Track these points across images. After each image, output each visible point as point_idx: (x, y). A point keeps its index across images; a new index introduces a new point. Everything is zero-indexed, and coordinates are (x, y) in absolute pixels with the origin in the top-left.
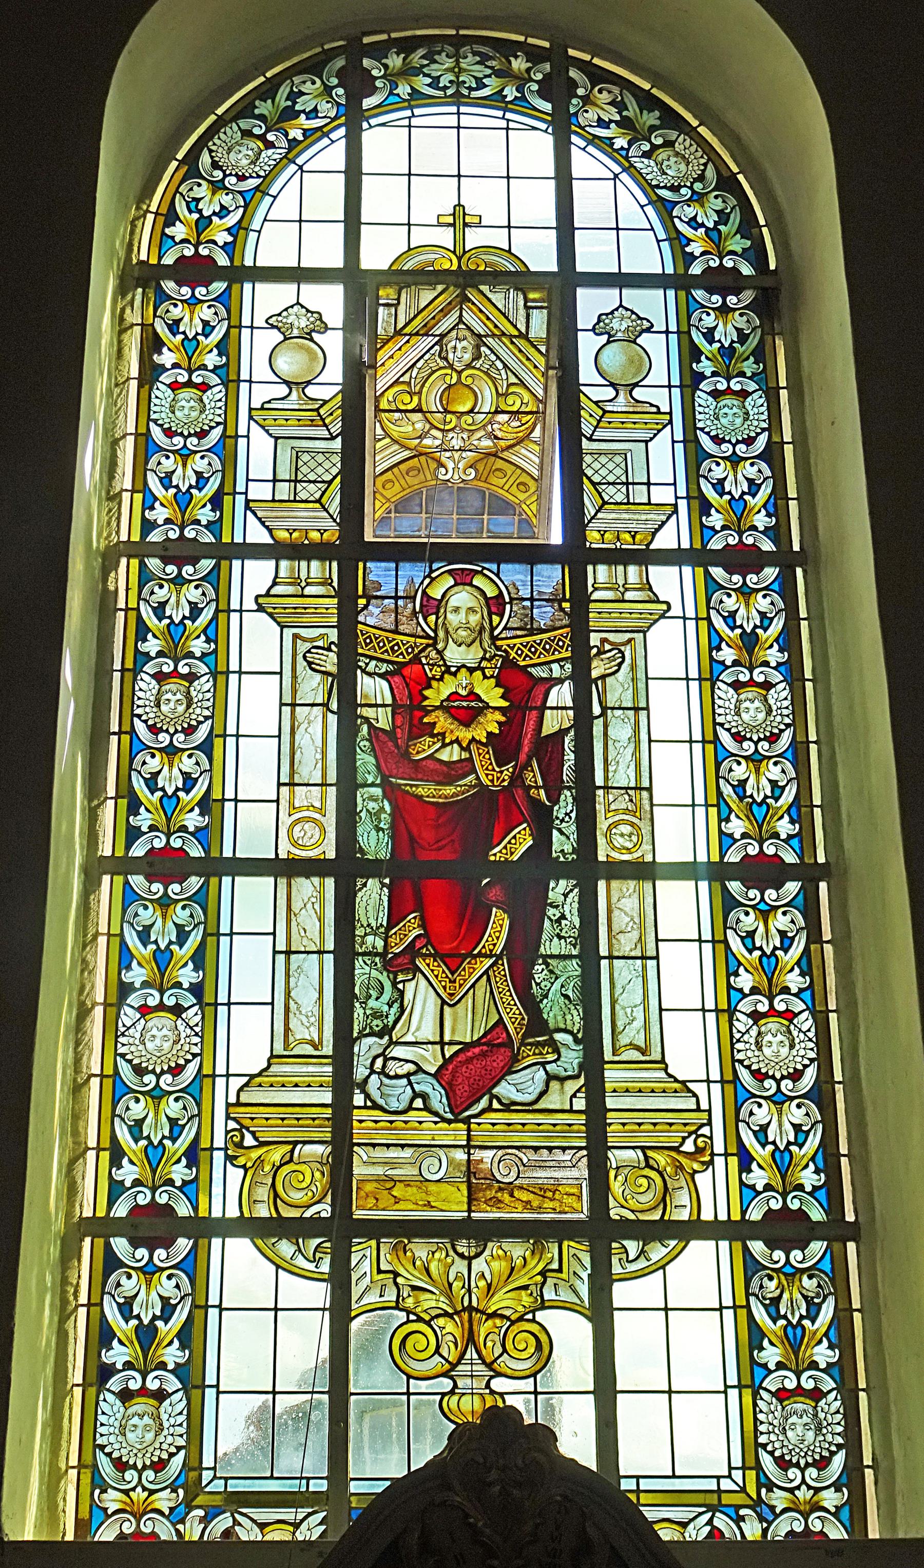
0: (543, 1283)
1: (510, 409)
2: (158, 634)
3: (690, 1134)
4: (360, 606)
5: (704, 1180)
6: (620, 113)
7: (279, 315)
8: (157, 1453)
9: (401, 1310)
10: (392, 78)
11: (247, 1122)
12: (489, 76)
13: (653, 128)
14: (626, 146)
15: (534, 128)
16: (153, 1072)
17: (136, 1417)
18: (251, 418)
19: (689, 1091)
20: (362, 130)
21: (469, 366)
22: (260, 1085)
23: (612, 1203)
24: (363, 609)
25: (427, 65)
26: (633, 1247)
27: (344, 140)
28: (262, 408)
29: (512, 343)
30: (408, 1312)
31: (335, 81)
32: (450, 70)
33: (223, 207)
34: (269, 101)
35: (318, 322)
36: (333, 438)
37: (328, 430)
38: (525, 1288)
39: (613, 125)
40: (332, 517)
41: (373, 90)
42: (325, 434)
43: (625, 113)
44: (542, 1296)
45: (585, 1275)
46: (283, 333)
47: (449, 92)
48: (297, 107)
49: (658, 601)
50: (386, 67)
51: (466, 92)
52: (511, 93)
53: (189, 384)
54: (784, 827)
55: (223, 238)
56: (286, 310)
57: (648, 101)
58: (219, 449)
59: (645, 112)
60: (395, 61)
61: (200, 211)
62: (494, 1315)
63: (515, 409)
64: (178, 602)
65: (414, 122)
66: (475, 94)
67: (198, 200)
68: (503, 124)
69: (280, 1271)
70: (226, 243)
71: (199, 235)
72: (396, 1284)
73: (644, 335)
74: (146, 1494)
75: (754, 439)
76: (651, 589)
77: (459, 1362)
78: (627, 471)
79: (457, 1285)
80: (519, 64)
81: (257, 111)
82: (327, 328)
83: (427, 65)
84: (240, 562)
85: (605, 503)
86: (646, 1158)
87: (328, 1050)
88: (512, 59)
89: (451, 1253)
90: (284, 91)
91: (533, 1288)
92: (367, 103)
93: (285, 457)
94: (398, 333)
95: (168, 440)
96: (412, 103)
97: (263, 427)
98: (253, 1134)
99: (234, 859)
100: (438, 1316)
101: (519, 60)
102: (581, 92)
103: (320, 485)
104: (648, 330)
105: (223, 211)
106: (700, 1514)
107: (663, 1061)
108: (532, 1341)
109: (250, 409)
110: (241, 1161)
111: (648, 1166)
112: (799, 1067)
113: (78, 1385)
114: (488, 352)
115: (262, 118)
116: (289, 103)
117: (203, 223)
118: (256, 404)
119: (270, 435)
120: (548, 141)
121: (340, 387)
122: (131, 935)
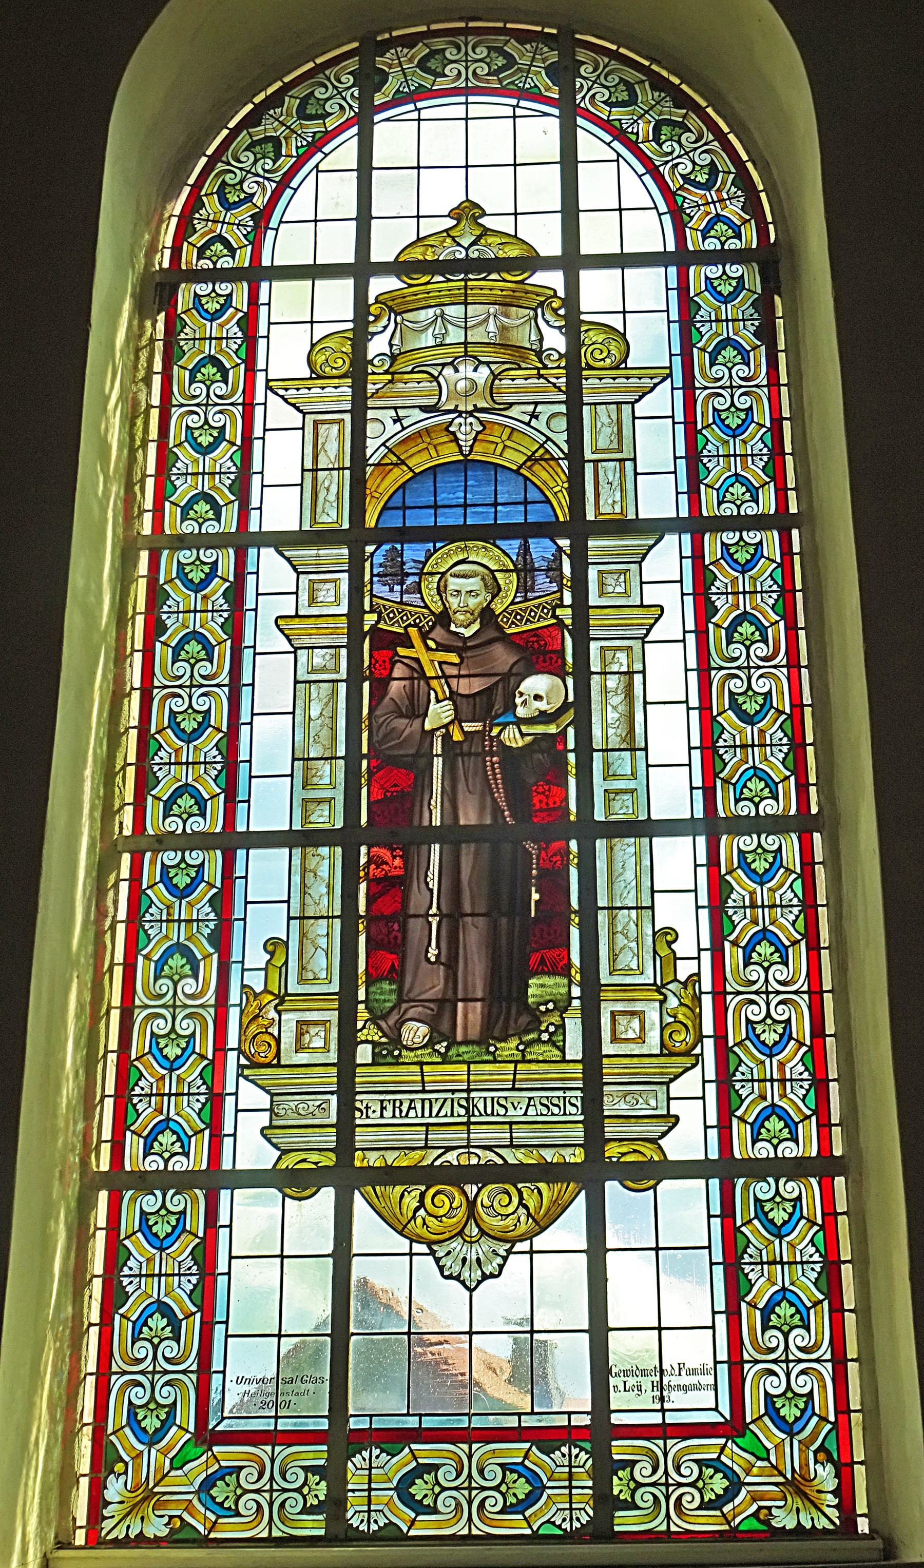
15: (546, 114)
69: (287, 1199)
99: (234, 1171)
113: (91, 1374)
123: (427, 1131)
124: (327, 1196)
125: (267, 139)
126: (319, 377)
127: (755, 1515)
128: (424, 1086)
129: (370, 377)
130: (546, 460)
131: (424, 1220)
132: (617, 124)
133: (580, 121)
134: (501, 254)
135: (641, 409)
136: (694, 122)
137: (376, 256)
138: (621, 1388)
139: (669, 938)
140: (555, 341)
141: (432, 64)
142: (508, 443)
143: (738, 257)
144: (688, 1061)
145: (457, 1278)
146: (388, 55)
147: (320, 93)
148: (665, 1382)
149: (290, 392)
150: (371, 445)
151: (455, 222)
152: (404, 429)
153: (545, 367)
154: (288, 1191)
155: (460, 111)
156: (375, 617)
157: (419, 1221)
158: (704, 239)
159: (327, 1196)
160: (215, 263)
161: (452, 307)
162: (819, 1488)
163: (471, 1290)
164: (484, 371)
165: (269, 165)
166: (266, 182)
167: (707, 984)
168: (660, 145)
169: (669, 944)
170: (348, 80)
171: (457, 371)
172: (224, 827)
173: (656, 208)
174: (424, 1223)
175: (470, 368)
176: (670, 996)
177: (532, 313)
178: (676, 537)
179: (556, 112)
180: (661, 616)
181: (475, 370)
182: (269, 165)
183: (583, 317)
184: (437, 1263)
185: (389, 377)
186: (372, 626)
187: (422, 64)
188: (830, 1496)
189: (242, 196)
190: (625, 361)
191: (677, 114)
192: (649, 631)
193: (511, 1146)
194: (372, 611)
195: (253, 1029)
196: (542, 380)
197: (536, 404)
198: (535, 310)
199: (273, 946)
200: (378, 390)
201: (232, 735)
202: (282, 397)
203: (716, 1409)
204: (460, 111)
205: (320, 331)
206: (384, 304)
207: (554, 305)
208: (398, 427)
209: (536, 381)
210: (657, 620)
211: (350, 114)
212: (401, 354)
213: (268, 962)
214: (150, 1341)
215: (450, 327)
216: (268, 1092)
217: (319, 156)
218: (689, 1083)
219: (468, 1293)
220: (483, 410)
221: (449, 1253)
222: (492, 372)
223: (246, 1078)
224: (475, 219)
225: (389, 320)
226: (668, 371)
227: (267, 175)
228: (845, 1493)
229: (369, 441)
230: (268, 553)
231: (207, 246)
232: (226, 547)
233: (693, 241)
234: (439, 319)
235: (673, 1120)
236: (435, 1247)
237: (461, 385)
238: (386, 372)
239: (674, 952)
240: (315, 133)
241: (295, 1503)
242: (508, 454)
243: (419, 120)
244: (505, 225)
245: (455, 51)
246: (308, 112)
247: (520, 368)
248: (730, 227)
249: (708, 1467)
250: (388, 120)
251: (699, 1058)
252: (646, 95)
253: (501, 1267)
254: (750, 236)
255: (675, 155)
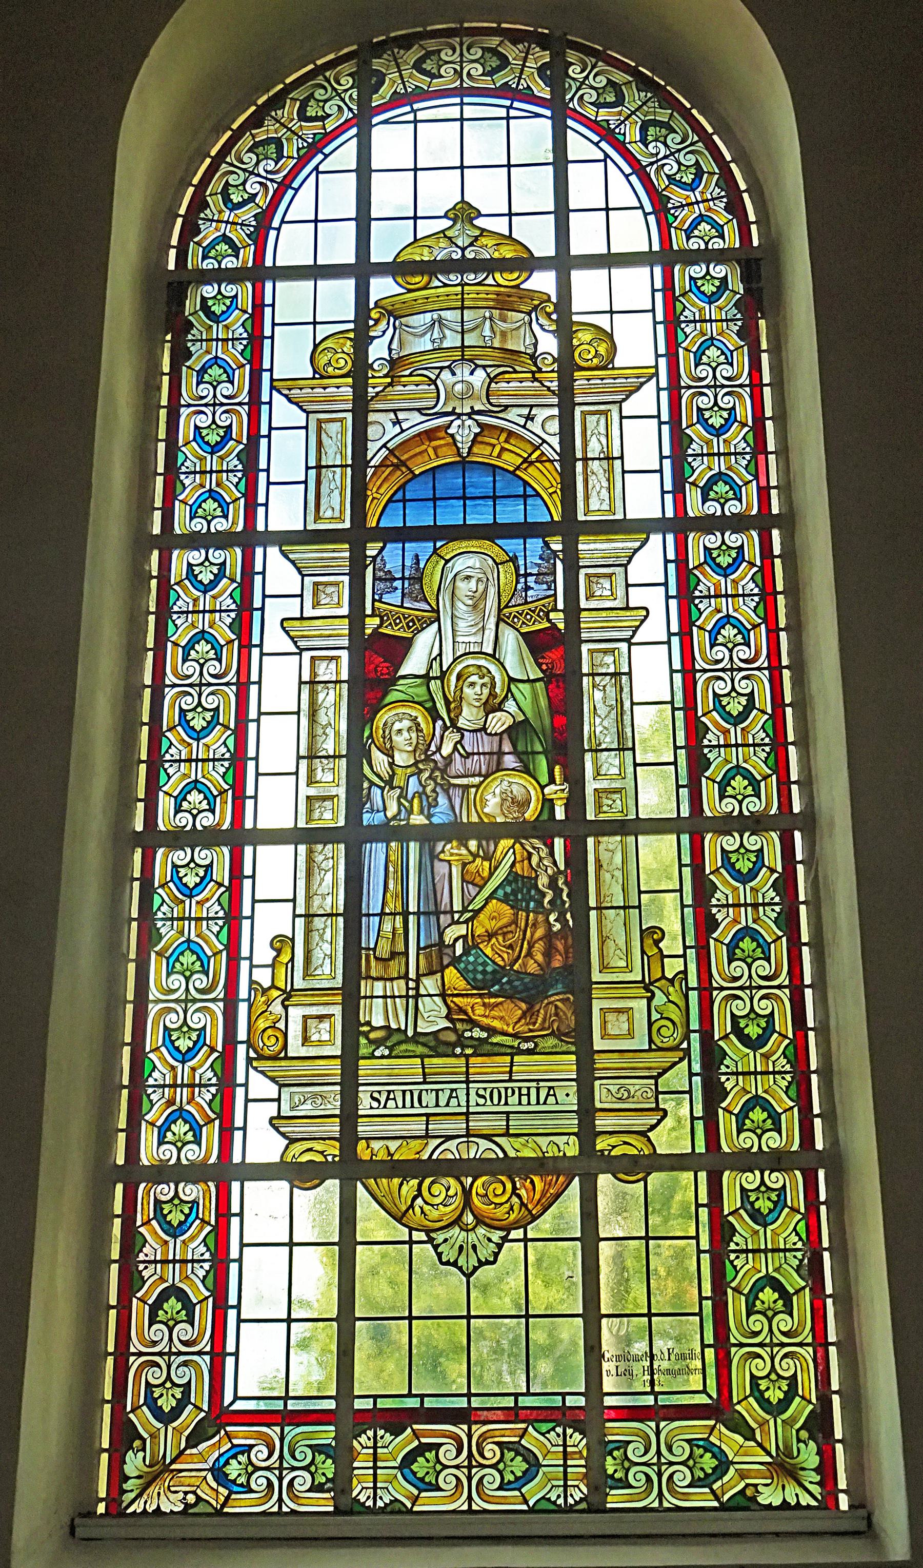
15: (538, 115)
27: (355, 139)
84: (251, 848)
123: (427, 1121)
124: (333, 1185)
125: (268, 141)
126: (322, 377)
127: (742, 1492)
128: (424, 1078)
129: (370, 381)
130: (541, 462)
131: (421, 1208)
132: (604, 124)
133: (570, 122)
134: (496, 255)
135: (628, 408)
136: (679, 123)
137: (376, 257)
138: (614, 1372)
139: (655, 936)
140: (549, 344)
141: (428, 65)
142: (507, 446)
143: (721, 256)
144: (674, 1056)
145: (455, 1264)
146: (385, 56)
147: (319, 94)
148: (655, 1366)
149: (293, 392)
150: (372, 447)
151: (451, 223)
152: (403, 431)
153: (540, 370)
154: (296, 1183)
155: (455, 112)
156: (377, 621)
157: (418, 1210)
158: (688, 239)
159: (333, 1185)
160: (220, 263)
161: (449, 312)
162: (803, 1465)
163: (468, 1276)
164: (480, 374)
165: (271, 165)
166: (269, 183)
167: (693, 982)
168: (646, 146)
169: (657, 943)
170: (347, 82)
171: (454, 374)
172: (232, 823)
173: (642, 207)
174: (422, 1212)
175: (467, 371)
176: (658, 993)
177: (527, 318)
178: (659, 537)
179: (548, 113)
180: (646, 617)
181: (472, 373)
182: (271, 165)
183: (575, 318)
184: (436, 1251)
185: (389, 380)
186: (375, 630)
187: (418, 66)
188: (813, 1473)
189: (246, 196)
190: (612, 361)
191: (663, 115)
192: (634, 632)
193: (507, 1134)
194: (373, 615)
195: (261, 1024)
196: (536, 384)
197: (531, 407)
198: (529, 314)
199: (280, 943)
200: (377, 393)
201: (240, 734)
202: (286, 396)
203: (704, 1391)
204: (455, 112)
205: (323, 331)
206: (383, 308)
207: (548, 310)
208: (397, 429)
209: (530, 384)
210: (642, 622)
211: (348, 115)
212: (400, 358)
213: (275, 958)
214: (166, 1324)
215: (447, 332)
216: (276, 1083)
217: (320, 157)
218: (677, 1078)
219: (464, 1279)
220: (480, 413)
221: (446, 1240)
222: (488, 375)
223: (255, 1069)
224: (471, 220)
225: (388, 323)
226: (653, 371)
227: (269, 176)
228: (826, 1470)
229: (369, 444)
230: (273, 552)
231: (212, 246)
232: (231, 546)
233: (678, 241)
234: (437, 324)
235: (661, 1113)
236: (433, 1235)
237: (458, 387)
238: (385, 376)
239: (660, 950)
240: (315, 134)
241: (303, 1481)
242: (506, 456)
243: (416, 122)
244: (500, 226)
245: (450, 52)
246: (308, 114)
247: (515, 372)
248: (713, 227)
249: (165, 1137)
250: (386, 122)
251: (687, 1052)
252: (634, 97)
253: (496, 1255)
254: (732, 239)
255: (660, 156)
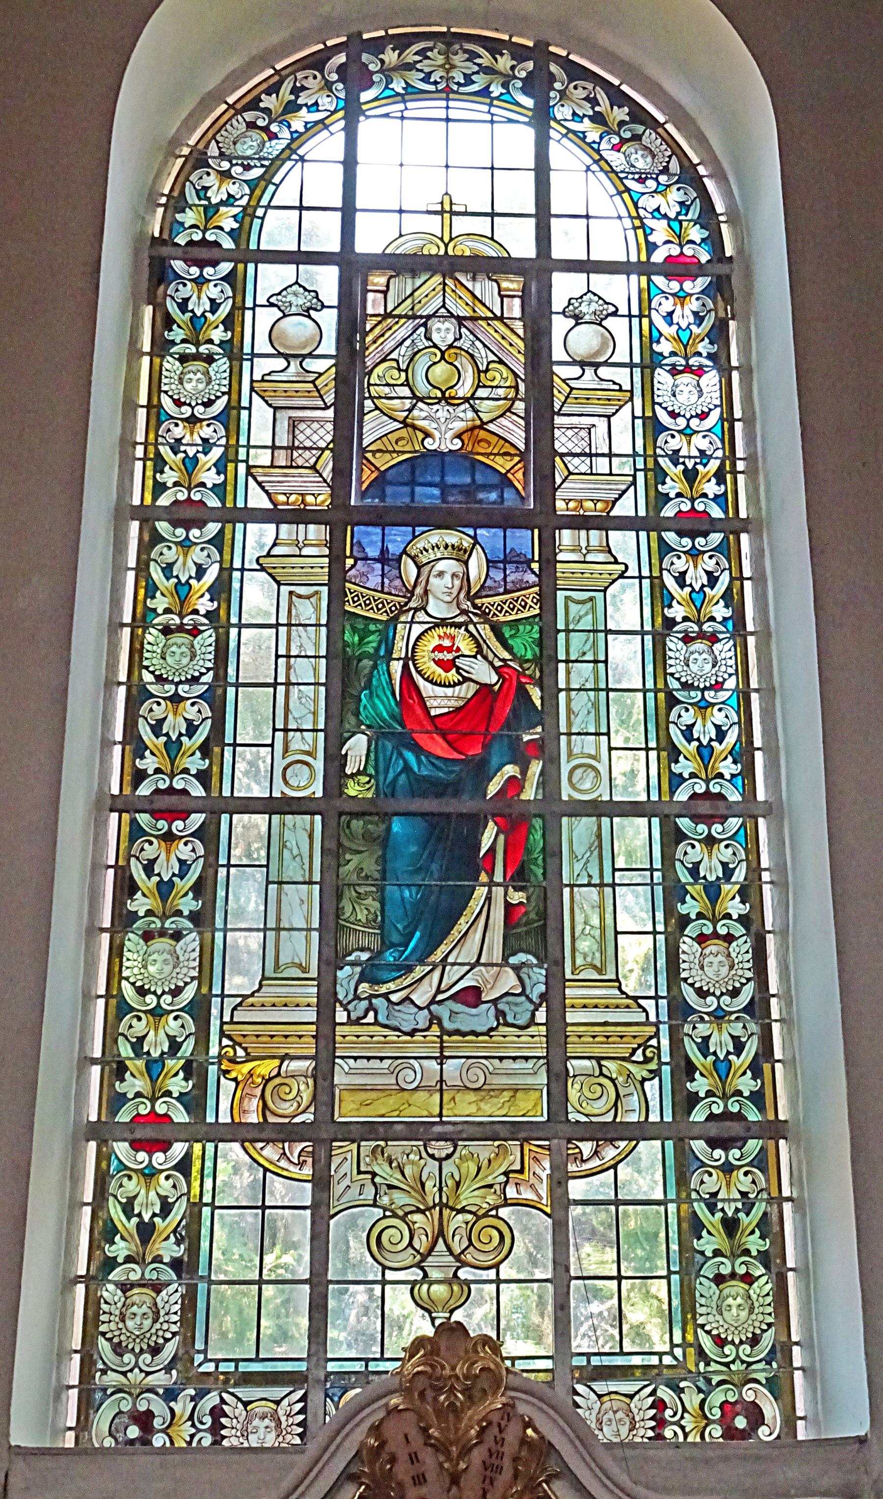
0: (507, 1182)
1: (489, 383)
2: (166, 593)
3: (639, 1046)
4: (348, 566)
5: (651, 1087)
6: (593, 108)
7: (279, 294)
8: (154, 1338)
9: (379, 1207)
10: (387, 72)
11: (239, 1039)
12: (477, 73)
13: (622, 123)
14: (598, 140)
16: (172, 682)
17: (135, 1307)
18: (252, 389)
19: (640, 1006)
20: (358, 121)
21: (451, 346)
22: (252, 1005)
23: (570, 1109)
24: (350, 569)
25: (420, 61)
26: (587, 1148)
28: (263, 380)
29: (489, 325)
30: (385, 1210)
31: (334, 77)
32: (442, 66)
33: (230, 196)
34: (274, 95)
35: (315, 300)
36: (327, 408)
37: (323, 400)
38: (490, 1186)
39: (586, 120)
40: (325, 481)
41: (371, 84)
42: (320, 403)
43: (597, 109)
44: (505, 1194)
45: (544, 1175)
46: (282, 311)
47: (440, 87)
48: (300, 101)
49: (616, 562)
50: (382, 62)
51: (455, 87)
52: (496, 90)
53: (181, 628)
54: (728, 768)
55: (229, 224)
56: (285, 289)
57: (618, 98)
58: (223, 418)
59: (615, 108)
60: (391, 57)
61: (208, 199)
62: (463, 1210)
63: (494, 384)
64: (184, 564)
65: (406, 114)
66: (462, 89)
67: (206, 189)
68: (489, 117)
70: (232, 230)
71: (207, 221)
72: (374, 1184)
73: (610, 318)
74: (143, 1375)
75: (708, 414)
76: (610, 552)
77: (429, 1254)
78: (590, 445)
79: (429, 1185)
80: (504, 62)
81: (262, 105)
82: (323, 306)
83: (420, 61)
85: (570, 473)
86: (600, 1066)
87: (314, 973)
88: (498, 56)
89: (424, 1155)
90: (287, 87)
91: (497, 1187)
92: (365, 96)
93: (283, 426)
94: (387, 315)
95: (177, 409)
96: (407, 97)
97: (263, 398)
98: (245, 1049)
100: (411, 1212)
101: (505, 57)
102: (557, 85)
103: (314, 452)
104: (615, 314)
105: (230, 200)
106: (645, 1386)
107: (617, 980)
108: (495, 1234)
109: (252, 381)
110: (233, 1075)
111: (601, 1074)
112: (737, 985)
114: (468, 333)
115: (267, 111)
116: (292, 97)
117: (211, 211)
118: (257, 376)
119: (270, 405)
120: (529, 134)
121: (333, 361)
122: (136, 866)
